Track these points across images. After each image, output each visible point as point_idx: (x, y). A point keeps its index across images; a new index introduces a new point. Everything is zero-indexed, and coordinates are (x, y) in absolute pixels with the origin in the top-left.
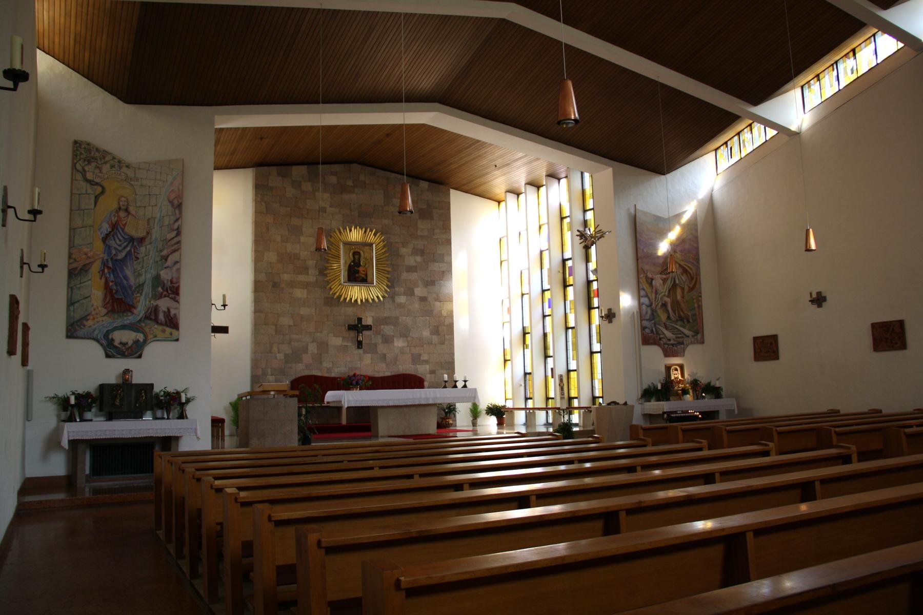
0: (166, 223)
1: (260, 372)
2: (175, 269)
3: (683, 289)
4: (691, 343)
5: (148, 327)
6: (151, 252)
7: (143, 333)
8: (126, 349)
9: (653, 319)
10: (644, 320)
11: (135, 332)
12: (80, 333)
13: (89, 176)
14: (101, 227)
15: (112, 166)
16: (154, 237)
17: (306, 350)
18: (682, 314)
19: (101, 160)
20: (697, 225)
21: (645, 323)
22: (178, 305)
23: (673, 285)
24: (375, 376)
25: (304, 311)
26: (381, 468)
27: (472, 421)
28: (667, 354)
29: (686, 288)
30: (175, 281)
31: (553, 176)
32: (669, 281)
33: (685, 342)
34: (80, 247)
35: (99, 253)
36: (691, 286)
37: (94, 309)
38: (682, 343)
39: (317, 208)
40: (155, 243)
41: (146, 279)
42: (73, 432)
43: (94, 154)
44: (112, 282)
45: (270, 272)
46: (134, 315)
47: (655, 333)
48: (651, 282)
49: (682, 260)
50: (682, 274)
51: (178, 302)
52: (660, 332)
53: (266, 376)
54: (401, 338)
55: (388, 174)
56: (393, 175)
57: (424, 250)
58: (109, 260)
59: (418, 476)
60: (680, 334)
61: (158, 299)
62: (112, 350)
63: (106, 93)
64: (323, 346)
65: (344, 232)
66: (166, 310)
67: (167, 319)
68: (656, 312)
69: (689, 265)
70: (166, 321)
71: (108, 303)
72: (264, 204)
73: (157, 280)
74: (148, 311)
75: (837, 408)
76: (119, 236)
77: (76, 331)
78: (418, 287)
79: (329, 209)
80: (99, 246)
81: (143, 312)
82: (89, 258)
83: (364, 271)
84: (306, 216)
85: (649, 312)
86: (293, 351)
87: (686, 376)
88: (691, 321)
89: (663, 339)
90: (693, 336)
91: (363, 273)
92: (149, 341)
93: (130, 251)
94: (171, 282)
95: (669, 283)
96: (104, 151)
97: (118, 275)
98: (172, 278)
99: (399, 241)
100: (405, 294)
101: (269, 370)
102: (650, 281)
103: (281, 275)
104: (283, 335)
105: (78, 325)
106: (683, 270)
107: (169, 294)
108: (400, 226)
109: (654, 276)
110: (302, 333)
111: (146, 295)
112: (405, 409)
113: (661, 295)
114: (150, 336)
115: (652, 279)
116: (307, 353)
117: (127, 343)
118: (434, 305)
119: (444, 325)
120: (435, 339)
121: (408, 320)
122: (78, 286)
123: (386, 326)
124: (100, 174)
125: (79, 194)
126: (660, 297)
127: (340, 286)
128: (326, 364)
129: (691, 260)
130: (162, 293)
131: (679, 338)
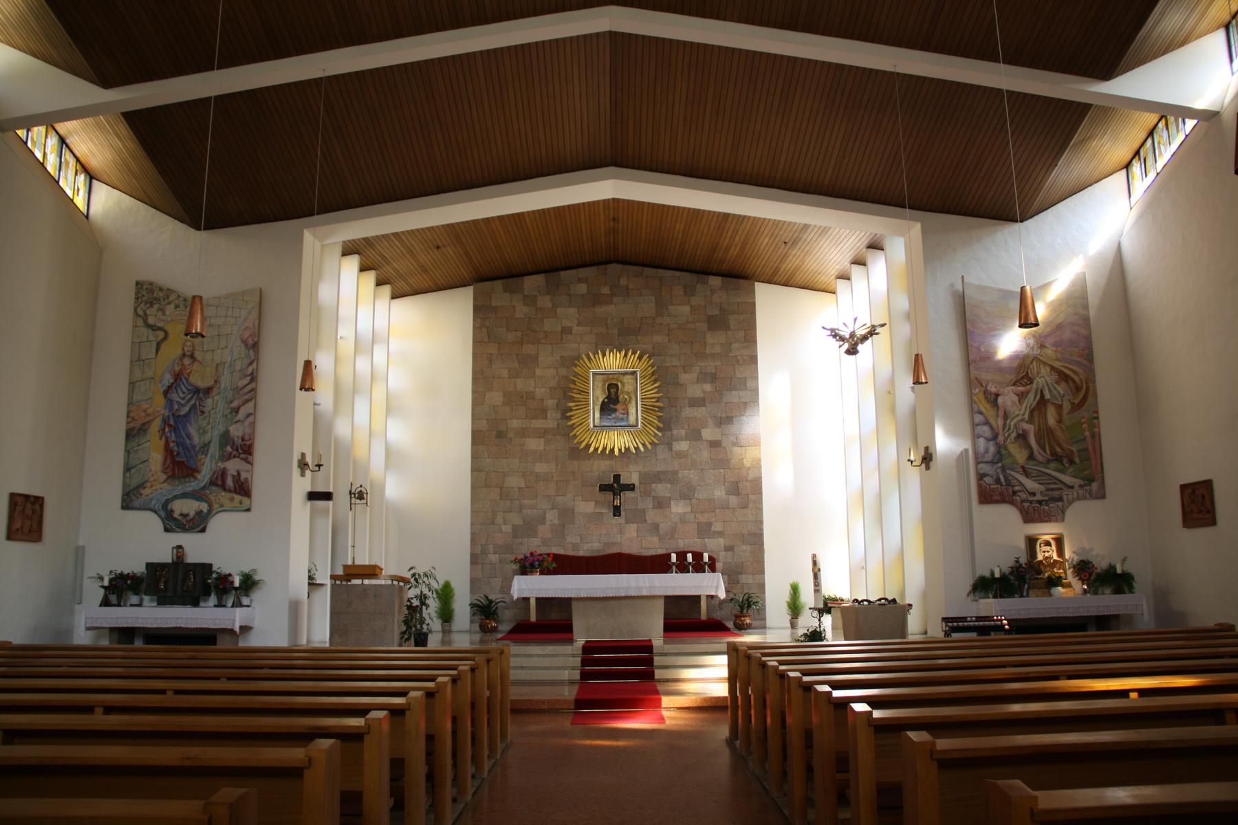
0: (238, 367)
1: (478, 550)
2: (247, 422)
3: (1059, 408)
4: (1079, 499)
5: (214, 494)
6: (219, 405)
7: (206, 501)
8: (187, 521)
9: (1000, 460)
10: (982, 462)
11: (198, 500)
12: (136, 503)
13: (151, 321)
14: (163, 379)
15: (177, 306)
16: (223, 386)
17: (542, 520)
18: (1058, 450)
19: (164, 299)
20: (1087, 298)
21: (985, 468)
22: (250, 466)
23: (1038, 403)
24: (643, 555)
25: (540, 468)
26: (229, 679)
27: (790, 620)
28: (1028, 518)
29: (1067, 406)
30: (247, 437)
31: (875, 246)
32: (1031, 396)
33: (1065, 498)
34: (138, 404)
35: (159, 409)
36: (1076, 401)
37: (153, 475)
38: (1060, 499)
39: (559, 329)
40: (224, 393)
41: (212, 437)
42: (92, 618)
43: (157, 294)
44: (173, 442)
45: (494, 417)
46: (197, 481)
47: (1004, 484)
48: (996, 400)
49: (1058, 360)
50: (1058, 383)
51: (251, 463)
52: (1014, 482)
53: (487, 555)
54: (682, 501)
55: (661, 272)
56: (669, 273)
57: (716, 374)
58: (171, 417)
59: (172, 692)
60: (1056, 484)
61: (226, 461)
62: (172, 523)
63: (176, 222)
64: (567, 515)
65: (595, 358)
66: (236, 474)
67: (237, 485)
68: (1005, 448)
69: (1071, 367)
70: (235, 488)
71: (169, 466)
72: (484, 330)
73: (225, 438)
74: (213, 475)
75: (1231, 622)
76: (183, 387)
77: (131, 500)
78: (706, 427)
79: (576, 329)
80: (160, 400)
81: (208, 477)
82: (148, 415)
84: (543, 341)
85: (992, 449)
86: (524, 521)
87: (1068, 554)
88: (1077, 460)
89: (1020, 494)
90: (1081, 486)
92: (215, 511)
93: (194, 405)
94: (243, 439)
95: (1031, 400)
96: (168, 289)
97: (180, 433)
98: (244, 434)
99: (678, 364)
100: (687, 438)
101: (491, 546)
102: (993, 399)
103: (509, 421)
104: (511, 500)
105: (133, 494)
106: (1059, 375)
107: (240, 453)
108: (679, 343)
109: (1001, 390)
110: (537, 497)
111: (211, 456)
112: (613, 602)
113: (1014, 421)
114: (216, 506)
115: (997, 395)
116: (544, 524)
117: (188, 515)
118: (731, 452)
119: (747, 481)
120: (733, 500)
121: (692, 475)
122: (135, 449)
123: (659, 485)
124: (164, 317)
125: (140, 343)
126: (1012, 423)
128: (572, 539)
129: (1077, 359)
130: (231, 453)
131: (1052, 489)
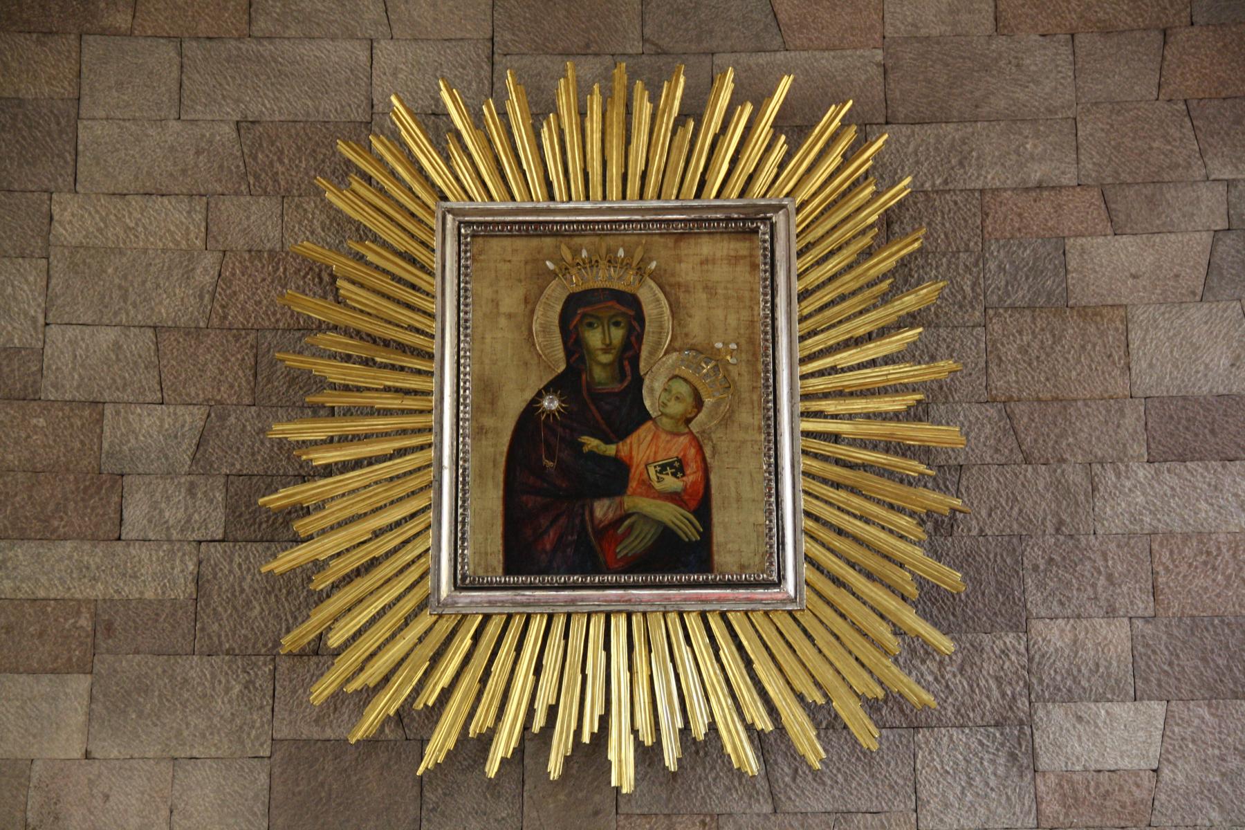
83: (678, 468)
91: (671, 483)
127: (426, 620)
